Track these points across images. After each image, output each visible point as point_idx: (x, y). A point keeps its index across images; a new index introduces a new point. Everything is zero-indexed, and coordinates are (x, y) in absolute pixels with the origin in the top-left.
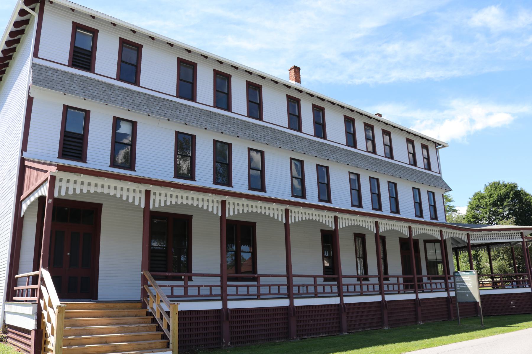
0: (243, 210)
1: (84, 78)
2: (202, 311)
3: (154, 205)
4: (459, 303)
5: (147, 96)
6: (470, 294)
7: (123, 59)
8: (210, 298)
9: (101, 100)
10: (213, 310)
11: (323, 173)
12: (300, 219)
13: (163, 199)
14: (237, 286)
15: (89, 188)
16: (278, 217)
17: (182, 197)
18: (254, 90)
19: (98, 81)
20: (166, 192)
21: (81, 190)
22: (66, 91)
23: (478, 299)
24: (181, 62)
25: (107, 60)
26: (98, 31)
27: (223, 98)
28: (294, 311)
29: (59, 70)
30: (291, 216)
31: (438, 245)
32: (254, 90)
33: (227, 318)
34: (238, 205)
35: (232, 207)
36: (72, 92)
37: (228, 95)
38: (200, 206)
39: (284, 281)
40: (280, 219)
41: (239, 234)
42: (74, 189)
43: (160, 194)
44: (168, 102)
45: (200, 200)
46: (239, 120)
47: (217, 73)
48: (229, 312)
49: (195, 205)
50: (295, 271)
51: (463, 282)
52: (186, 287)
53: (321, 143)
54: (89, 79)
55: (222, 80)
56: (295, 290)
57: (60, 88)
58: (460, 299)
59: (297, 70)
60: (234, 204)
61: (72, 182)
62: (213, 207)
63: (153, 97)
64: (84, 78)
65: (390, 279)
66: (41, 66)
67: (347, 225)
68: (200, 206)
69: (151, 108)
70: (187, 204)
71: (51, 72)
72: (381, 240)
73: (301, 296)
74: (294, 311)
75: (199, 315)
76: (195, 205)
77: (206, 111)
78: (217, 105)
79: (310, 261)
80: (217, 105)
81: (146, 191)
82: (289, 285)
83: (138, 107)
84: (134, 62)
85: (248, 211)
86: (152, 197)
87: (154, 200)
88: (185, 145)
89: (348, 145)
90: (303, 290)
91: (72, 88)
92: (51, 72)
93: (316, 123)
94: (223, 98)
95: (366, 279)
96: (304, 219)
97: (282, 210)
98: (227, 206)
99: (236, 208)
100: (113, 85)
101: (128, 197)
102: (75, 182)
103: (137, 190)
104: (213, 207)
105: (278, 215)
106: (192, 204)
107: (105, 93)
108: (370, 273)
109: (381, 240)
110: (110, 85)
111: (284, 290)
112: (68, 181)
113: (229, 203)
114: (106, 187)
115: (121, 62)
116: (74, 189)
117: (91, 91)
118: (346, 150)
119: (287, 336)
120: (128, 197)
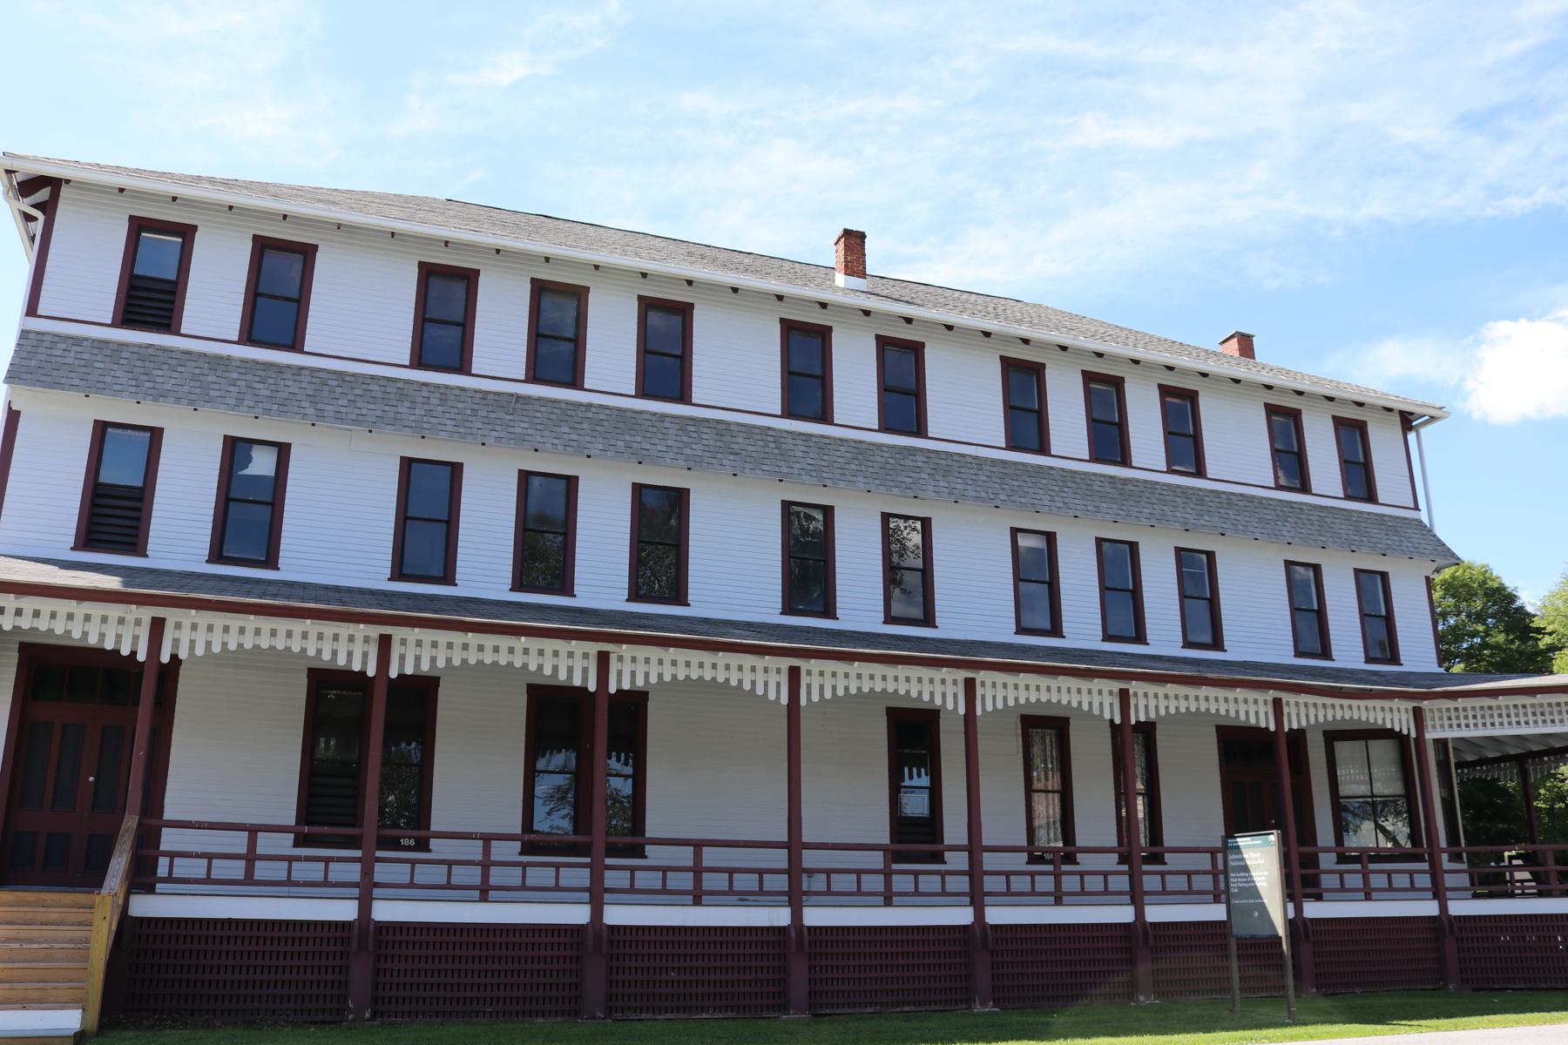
0: (847, 689)
1: (321, 375)
2: (865, 928)
3: (619, 681)
4: (1238, 939)
5: (321, 375)
6: (1262, 908)
7: (650, 347)
8: (759, 896)
9: (178, 400)
10: (949, 927)
11: (1199, 580)
12: (828, 695)
13: (1000, 694)
14: (916, 874)
15: (480, 656)
16: (1102, 710)
17: (688, 664)
18: (1181, 407)
19: (189, 353)
20: (337, 631)
21: (225, 644)
22: (89, 386)
23: (1281, 930)
24: (1008, 364)
25: (501, 335)
26: (691, 306)
27: (1109, 438)
28: (1146, 933)
29: (86, 339)
30: (983, 697)
31: (1382, 751)
32: (1181, 407)
33: (1452, 932)
34: (1166, 697)
35: (1142, 702)
36: (100, 391)
37: (1041, 416)
38: (734, 683)
39: (780, 858)
40: (772, 696)
41: (583, 733)
42: (209, 644)
43: (994, 685)
44: (383, 382)
45: (1074, 691)
46: (607, 408)
47: (1339, 422)
48: (605, 935)
49: (721, 680)
50: (808, 836)
51: (1246, 869)
52: (1058, 876)
53: (905, 448)
54: (164, 350)
55: (1105, 392)
56: (991, 883)
57: (76, 382)
58: (1241, 929)
59: (853, 241)
60: (1146, 695)
61: (734, 668)
62: (766, 684)
63: (340, 375)
64: (151, 351)
65: (434, 843)
66: (43, 334)
67: (1000, 706)
68: (734, 683)
69: (320, 406)
70: (288, 649)
71: (63, 346)
72: (1135, 744)
73: (830, 895)
74: (1146, 933)
75: (846, 937)
76: (721, 680)
77: (499, 394)
78: (1096, 456)
79: (852, 803)
80: (1096, 456)
81: (600, 653)
82: (794, 871)
83: (283, 407)
84: (817, 371)
85: (859, 689)
86: (979, 691)
87: (809, 686)
88: (1036, 573)
89: (1348, 497)
90: (1094, 883)
91: (108, 379)
92: (63, 346)
93: (1346, 463)
94: (1109, 438)
95: (1070, 858)
96: (840, 692)
97: (955, 682)
98: (1133, 701)
99: (1000, 694)
100: (229, 358)
101: (753, 683)
102: (661, 662)
103: (130, 618)
104: (766, 684)
105: (1257, 713)
106: (896, 691)
107: (204, 379)
108: (1084, 836)
109: (1135, 744)
110: (221, 357)
111: (780, 882)
112: (647, 661)
113: (1136, 694)
114: (45, 615)
115: (646, 352)
116: (209, 644)
117: (159, 380)
118: (1004, 462)
119: (572, 1007)
120: (753, 683)
